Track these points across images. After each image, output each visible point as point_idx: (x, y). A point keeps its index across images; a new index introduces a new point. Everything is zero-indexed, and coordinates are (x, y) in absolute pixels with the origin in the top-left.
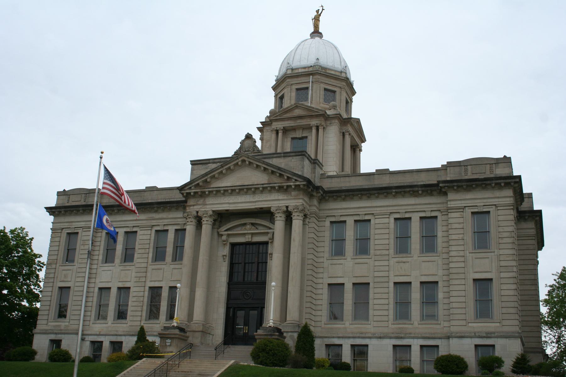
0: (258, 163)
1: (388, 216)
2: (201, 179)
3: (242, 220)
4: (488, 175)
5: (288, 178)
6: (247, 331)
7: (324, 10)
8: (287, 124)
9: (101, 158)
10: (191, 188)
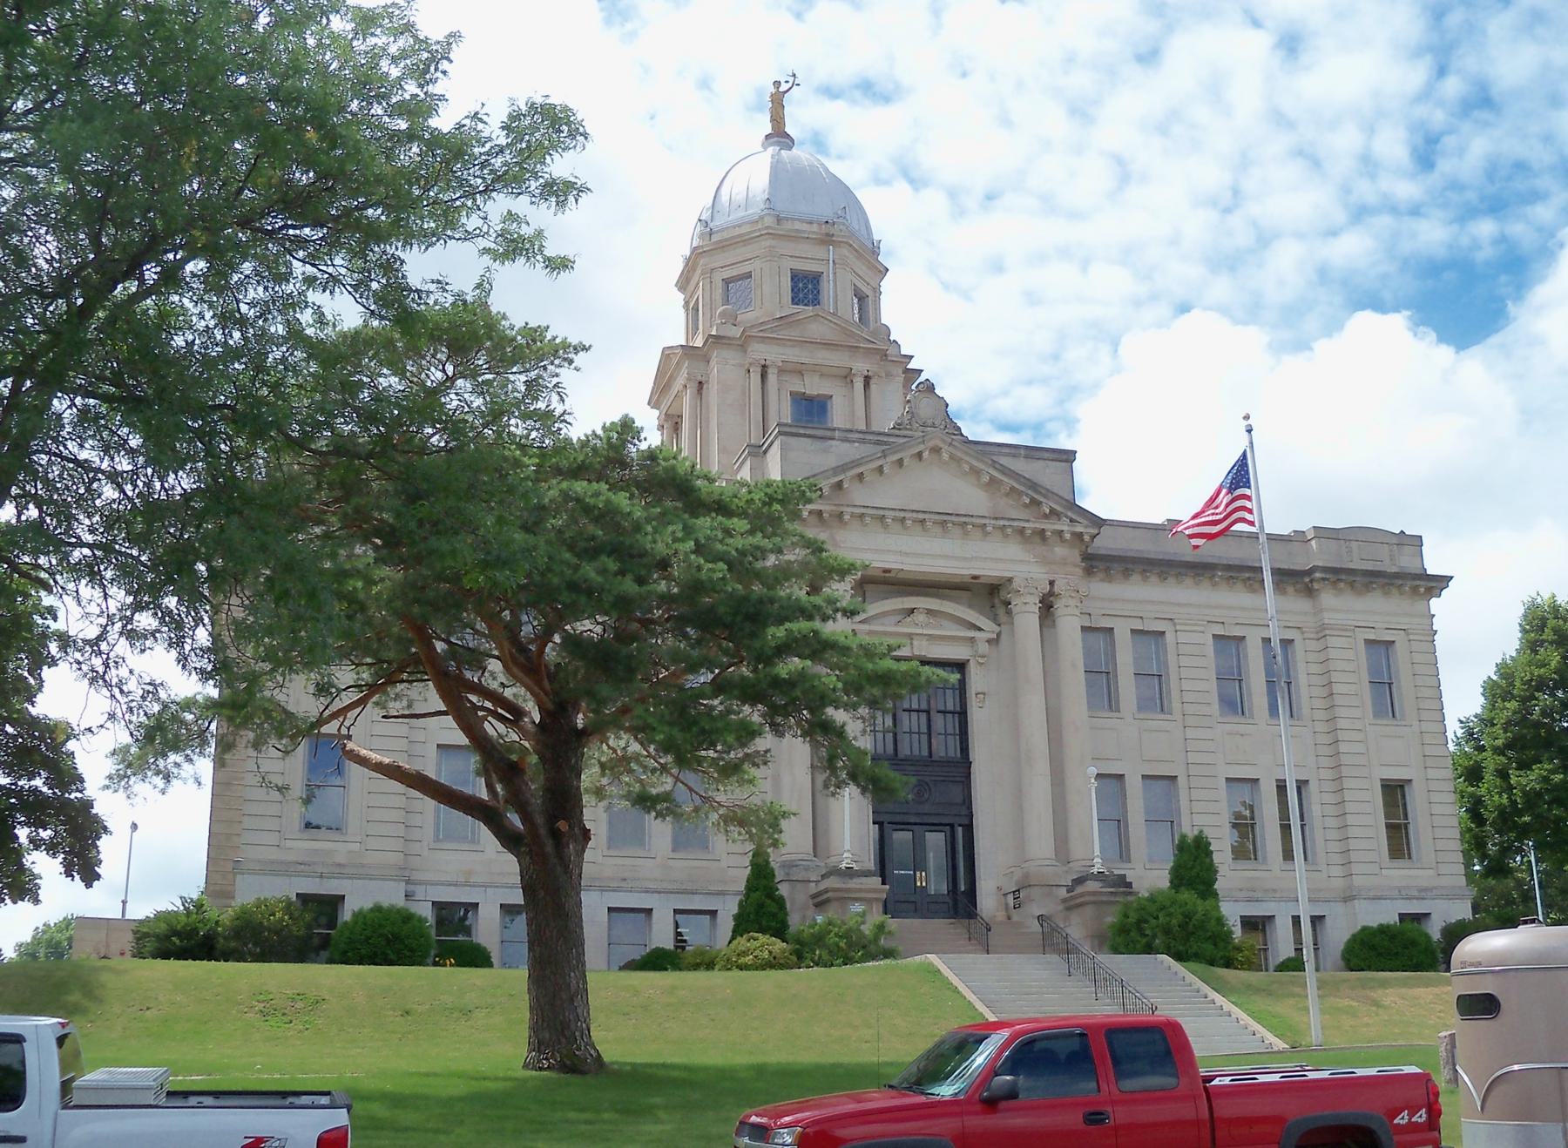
0: (975, 463)
3: (905, 599)
5: (1053, 512)
6: (924, 884)
7: (798, 85)
8: (794, 355)
9: (1249, 431)
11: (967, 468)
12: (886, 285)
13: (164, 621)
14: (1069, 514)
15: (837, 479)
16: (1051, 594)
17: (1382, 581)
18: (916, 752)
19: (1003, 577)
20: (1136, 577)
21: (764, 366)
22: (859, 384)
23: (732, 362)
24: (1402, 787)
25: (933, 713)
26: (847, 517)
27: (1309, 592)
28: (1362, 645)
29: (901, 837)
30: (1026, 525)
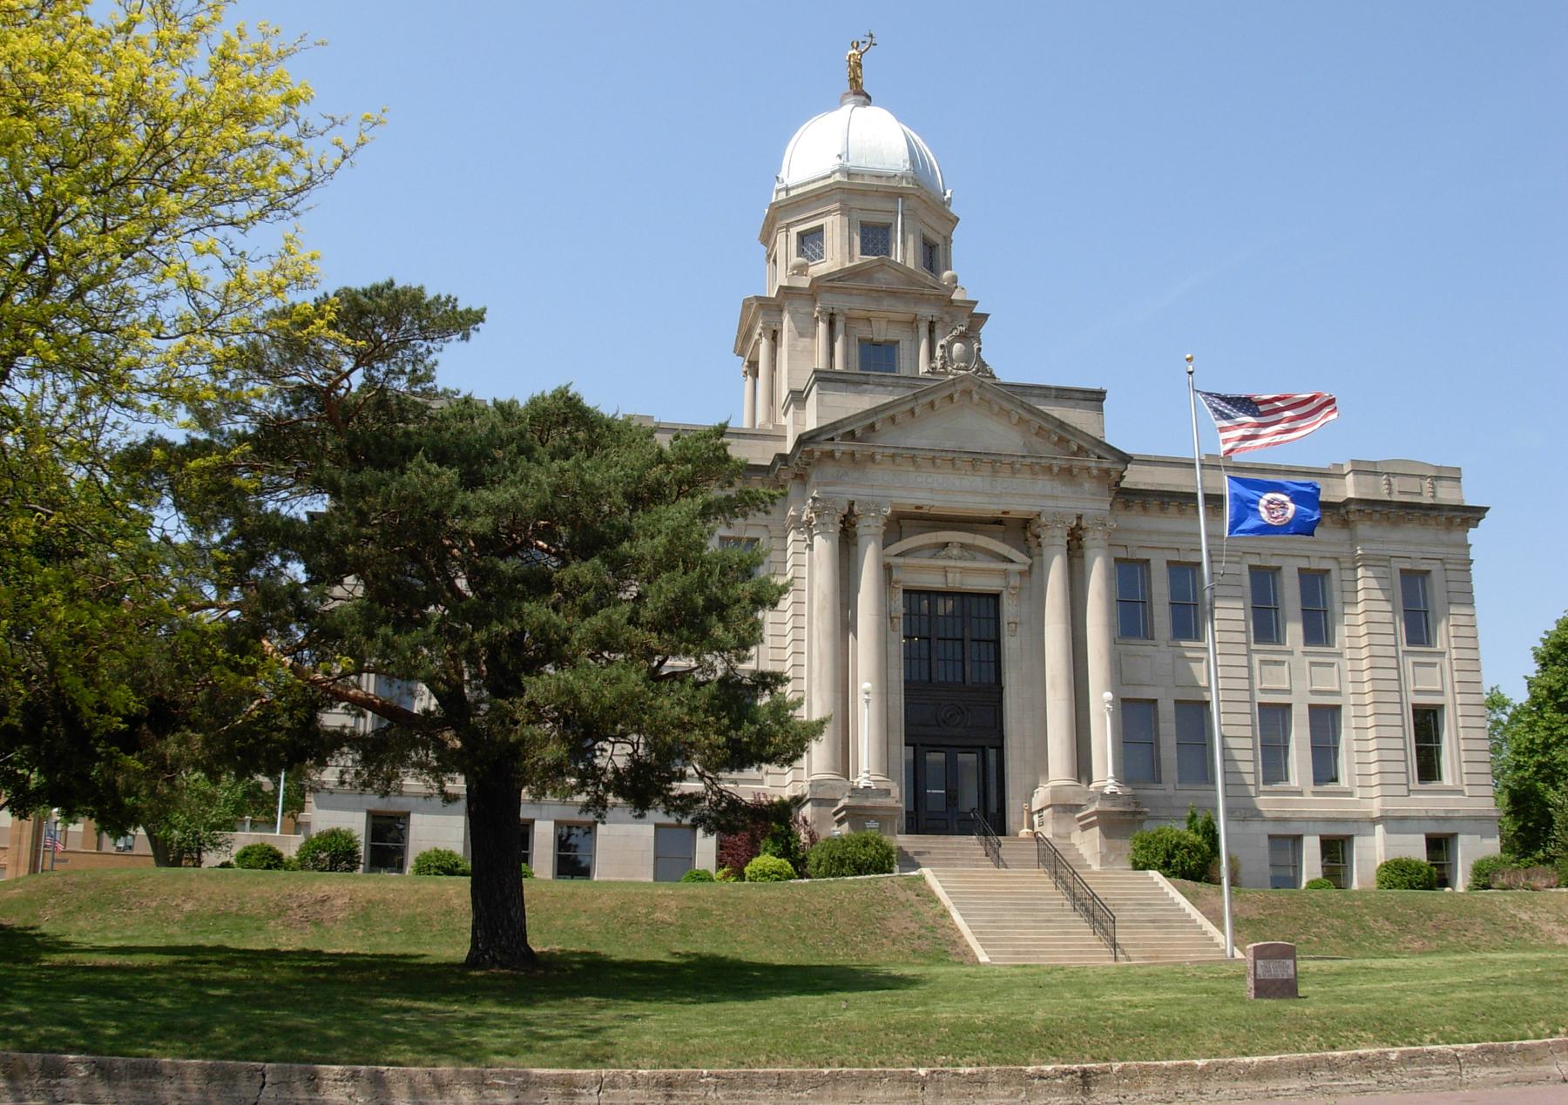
1: (1237, 559)
2: (860, 420)
4: (1426, 499)
10: (832, 439)
11: (996, 408)
12: (957, 235)
13: (572, 512)
14: (1097, 451)
15: (870, 421)
16: (1079, 527)
17: (1417, 513)
18: (950, 679)
19: (1031, 513)
20: (1172, 509)
21: (832, 314)
22: (923, 330)
23: (802, 311)
24: (1343, 841)
25: (967, 642)
26: (878, 457)
27: (1346, 523)
28: (1397, 576)
29: (936, 758)
30: (1054, 462)
